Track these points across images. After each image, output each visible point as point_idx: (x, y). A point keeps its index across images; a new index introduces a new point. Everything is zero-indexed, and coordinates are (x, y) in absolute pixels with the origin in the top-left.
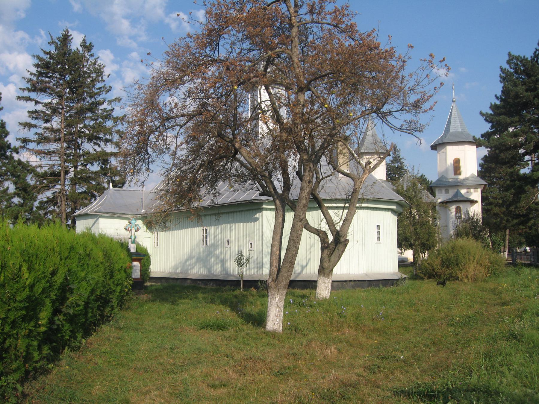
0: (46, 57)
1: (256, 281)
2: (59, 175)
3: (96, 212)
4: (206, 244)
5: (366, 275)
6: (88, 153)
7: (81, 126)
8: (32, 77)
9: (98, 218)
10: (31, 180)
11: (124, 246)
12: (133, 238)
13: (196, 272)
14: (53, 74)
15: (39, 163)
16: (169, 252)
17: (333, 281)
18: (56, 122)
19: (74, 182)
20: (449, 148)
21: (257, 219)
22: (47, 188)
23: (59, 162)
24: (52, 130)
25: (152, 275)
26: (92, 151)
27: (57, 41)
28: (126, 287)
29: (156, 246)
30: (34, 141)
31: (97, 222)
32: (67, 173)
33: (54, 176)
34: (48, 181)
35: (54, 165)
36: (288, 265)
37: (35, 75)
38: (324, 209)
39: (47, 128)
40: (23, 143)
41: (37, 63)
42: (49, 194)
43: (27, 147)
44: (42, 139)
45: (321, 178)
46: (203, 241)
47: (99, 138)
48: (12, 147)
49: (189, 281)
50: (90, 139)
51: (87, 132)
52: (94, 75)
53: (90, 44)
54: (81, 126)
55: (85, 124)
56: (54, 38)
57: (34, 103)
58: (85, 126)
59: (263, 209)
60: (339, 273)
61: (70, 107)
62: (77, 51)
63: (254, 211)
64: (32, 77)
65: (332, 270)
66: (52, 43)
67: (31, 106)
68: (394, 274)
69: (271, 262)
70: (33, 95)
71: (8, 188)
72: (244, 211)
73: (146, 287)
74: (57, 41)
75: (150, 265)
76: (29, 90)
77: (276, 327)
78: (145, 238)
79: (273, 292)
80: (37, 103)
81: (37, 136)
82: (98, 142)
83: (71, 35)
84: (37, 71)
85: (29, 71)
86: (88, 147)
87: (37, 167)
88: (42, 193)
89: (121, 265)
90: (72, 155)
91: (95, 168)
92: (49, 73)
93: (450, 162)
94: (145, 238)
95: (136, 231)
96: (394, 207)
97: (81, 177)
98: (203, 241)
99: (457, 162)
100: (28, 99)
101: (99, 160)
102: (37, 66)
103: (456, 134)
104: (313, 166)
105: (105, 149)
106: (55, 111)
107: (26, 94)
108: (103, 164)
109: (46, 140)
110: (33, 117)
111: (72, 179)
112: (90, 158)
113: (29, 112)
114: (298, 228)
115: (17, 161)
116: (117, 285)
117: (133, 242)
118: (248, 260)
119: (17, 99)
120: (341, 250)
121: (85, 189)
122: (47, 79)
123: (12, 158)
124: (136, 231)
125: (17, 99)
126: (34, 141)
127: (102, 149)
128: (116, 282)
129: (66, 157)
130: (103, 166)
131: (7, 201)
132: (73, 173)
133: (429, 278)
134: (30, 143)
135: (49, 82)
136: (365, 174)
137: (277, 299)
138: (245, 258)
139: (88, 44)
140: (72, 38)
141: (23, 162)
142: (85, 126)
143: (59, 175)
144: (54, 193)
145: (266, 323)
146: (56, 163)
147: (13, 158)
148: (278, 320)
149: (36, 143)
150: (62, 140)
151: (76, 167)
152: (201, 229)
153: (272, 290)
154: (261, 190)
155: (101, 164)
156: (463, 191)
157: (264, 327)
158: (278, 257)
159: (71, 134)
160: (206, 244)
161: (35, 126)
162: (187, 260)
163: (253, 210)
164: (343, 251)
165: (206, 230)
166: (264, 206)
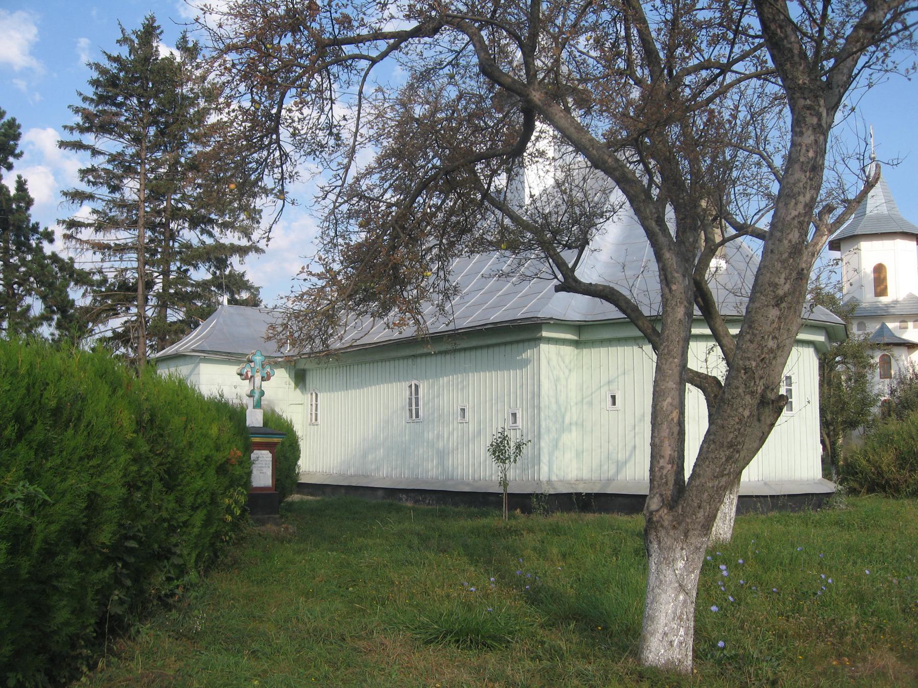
0: (112, 67)
1: (528, 496)
2: (134, 288)
3: (194, 351)
4: (417, 416)
5: (765, 484)
6: (188, 246)
7: (178, 196)
8: (86, 105)
9: (199, 363)
10: (79, 297)
11: (236, 415)
12: (257, 396)
13: (386, 472)
14: (126, 98)
15: (98, 265)
16: (341, 431)
17: (740, 497)
18: (131, 188)
19: (164, 302)
20: (864, 245)
21: (526, 362)
22: (113, 312)
23: (135, 265)
24: (123, 204)
25: (303, 480)
26: (195, 242)
27: (133, 37)
28: (229, 510)
29: (315, 419)
30: (90, 225)
31: (196, 372)
32: (149, 285)
33: (124, 293)
34: (113, 301)
35: (126, 269)
36: (723, 455)
37: (92, 100)
38: (719, 322)
39: (113, 201)
40: (69, 228)
41: (95, 77)
42: (116, 323)
43: (79, 236)
44: (104, 223)
45: (718, 239)
46: (411, 411)
47: (211, 221)
48: (41, 229)
49: (380, 493)
50: (195, 222)
51: (188, 207)
52: (202, 103)
53: (196, 45)
54: (178, 196)
55: (184, 194)
56: (128, 32)
57: (89, 152)
58: (185, 198)
59: (541, 339)
60: (754, 478)
61: (156, 160)
62: (170, 60)
63: (521, 345)
64: (86, 105)
65: (741, 472)
66: (125, 40)
67: (84, 160)
68: (808, 482)
69: (653, 445)
70: (89, 139)
71: (29, 307)
72: (498, 345)
73: (291, 504)
74: (133, 37)
75: (298, 458)
76: (82, 130)
77: (676, 654)
78: (282, 394)
79: (668, 542)
80: (95, 152)
81: (95, 216)
82: (209, 228)
83: (159, 27)
84: (96, 94)
85: (81, 94)
86: (190, 236)
87: (94, 273)
88: (103, 322)
89: (206, 452)
90: (159, 250)
91: (201, 274)
92: (118, 95)
93: (868, 268)
94: (282, 394)
95: (263, 379)
96: (820, 338)
97: (176, 293)
98: (411, 411)
99: (879, 270)
100: (78, 146)
101: (209, 260)
102: (95, 83)
103: (879, 218)
104: (827, 113)
105: (222, 241)
106: (129, 171)
107: (76, 136)
108: (217, 268)
109: (114, 224)
110: (89, 181)
111: (158, 296)
112: (193, 256)
113: (81, 171)
114: (767, 328)
115: (50, 257)
116: (195, 508)
117: (258, 405)
118: (519, 447)
119: (60, 147)
120: (769, 422)
121: (182, 314)
122: (114, 108)
123: (40, 249)
124: (263, 379)
125: (60, 147)
126: (90, 225)
127: (216, 240)
128: (189, 500)
129: (146, 252)
130: (218, 272)
131: (28, 331)
132: (161, 285)
133: (871, 490)
134: (83, 229)
135: (117, 114)
136: (822, 235)
137: (680, 564)
138: (512, 444)
139: (190, 45)
140: (162, 32)
141: (63, 260)
142: (185, 198)
143: (134, 288)
144: (126, 322)
145: (644, 639)
146: (129, 267)
147: (41, 249)
148: (682, 632)
149: (92, 229)
150: (141, 222)
151: (166, 273)
152: (405, 385)
153: (662, 533)
154: (560, 276)
155: (213, 268)
156: (891, 325)
157: (636, 652)
158: (676, 430)
159: (159, 213)
160: (417, 416)
161: (91, 197)
162: (365, 456)
163: (518, 342)
164: (772, 425)
165: (417, 387)
166: (545, 334)
